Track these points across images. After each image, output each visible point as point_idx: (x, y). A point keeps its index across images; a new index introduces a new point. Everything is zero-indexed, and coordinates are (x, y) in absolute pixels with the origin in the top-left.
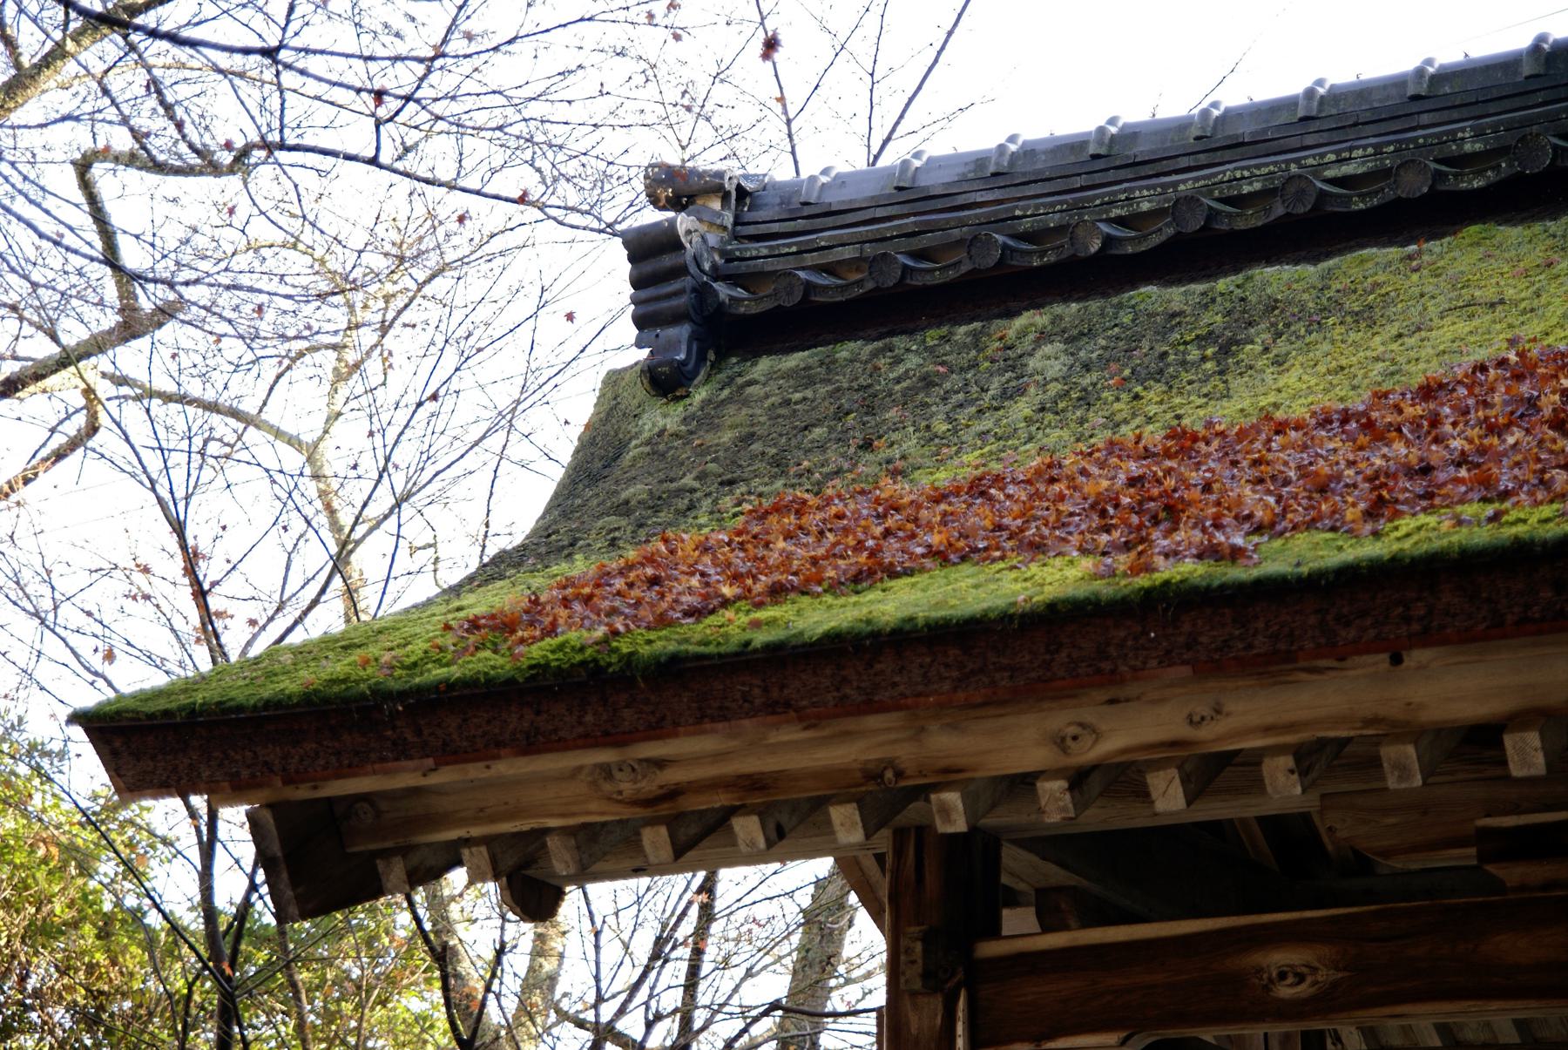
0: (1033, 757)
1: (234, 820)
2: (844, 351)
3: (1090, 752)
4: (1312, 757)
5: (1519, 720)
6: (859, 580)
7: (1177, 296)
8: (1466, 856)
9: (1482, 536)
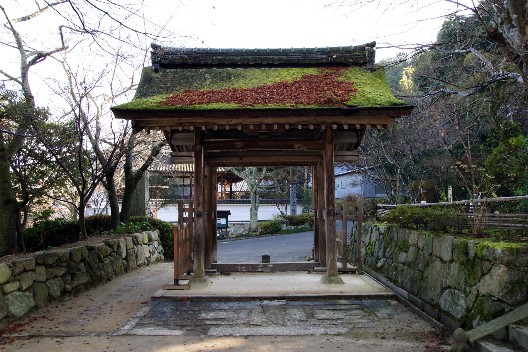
0: (224, 123)
1: (130, 121)
2: (179, 70)
3: (231, 123)
4: (255, 125)
5: (275, 124)
6: (208, 103)
7: (219, 70)
8: (257, 134)
9: (277, 107)
